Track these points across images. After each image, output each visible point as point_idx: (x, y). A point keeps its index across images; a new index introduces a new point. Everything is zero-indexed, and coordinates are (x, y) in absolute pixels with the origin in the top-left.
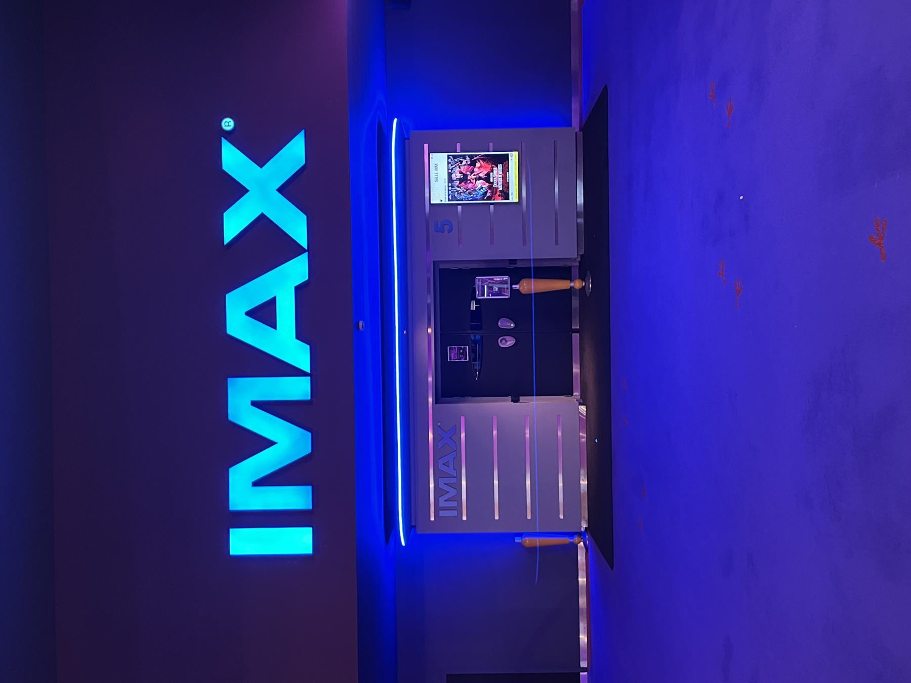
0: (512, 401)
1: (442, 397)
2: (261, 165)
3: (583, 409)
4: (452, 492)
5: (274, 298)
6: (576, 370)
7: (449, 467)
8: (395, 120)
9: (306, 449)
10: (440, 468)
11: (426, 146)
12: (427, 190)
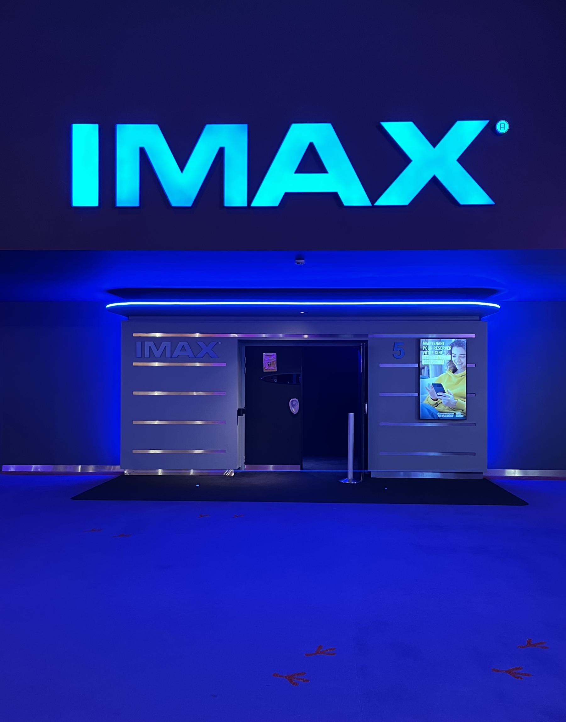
0: (239, 409)
1: (247, 348)
2: (461, 160)
3: (230, 473)
4: (157, 354)
5: (324, 170)
6: (271, 468)
7: (181, 351)
8: (498, 306)
9: (176, 200)
10: (180, 342)
11: (474, 336)
12: (434, 336)
